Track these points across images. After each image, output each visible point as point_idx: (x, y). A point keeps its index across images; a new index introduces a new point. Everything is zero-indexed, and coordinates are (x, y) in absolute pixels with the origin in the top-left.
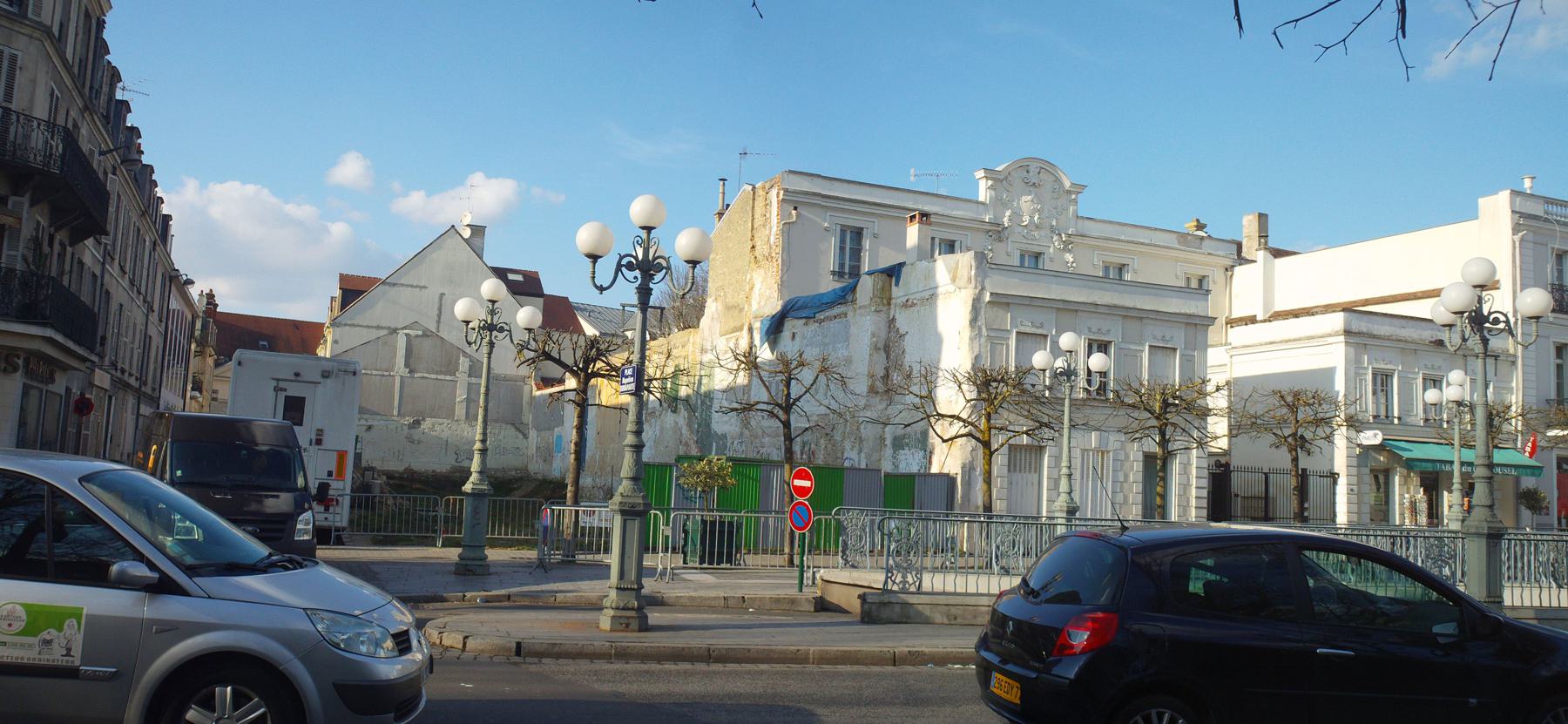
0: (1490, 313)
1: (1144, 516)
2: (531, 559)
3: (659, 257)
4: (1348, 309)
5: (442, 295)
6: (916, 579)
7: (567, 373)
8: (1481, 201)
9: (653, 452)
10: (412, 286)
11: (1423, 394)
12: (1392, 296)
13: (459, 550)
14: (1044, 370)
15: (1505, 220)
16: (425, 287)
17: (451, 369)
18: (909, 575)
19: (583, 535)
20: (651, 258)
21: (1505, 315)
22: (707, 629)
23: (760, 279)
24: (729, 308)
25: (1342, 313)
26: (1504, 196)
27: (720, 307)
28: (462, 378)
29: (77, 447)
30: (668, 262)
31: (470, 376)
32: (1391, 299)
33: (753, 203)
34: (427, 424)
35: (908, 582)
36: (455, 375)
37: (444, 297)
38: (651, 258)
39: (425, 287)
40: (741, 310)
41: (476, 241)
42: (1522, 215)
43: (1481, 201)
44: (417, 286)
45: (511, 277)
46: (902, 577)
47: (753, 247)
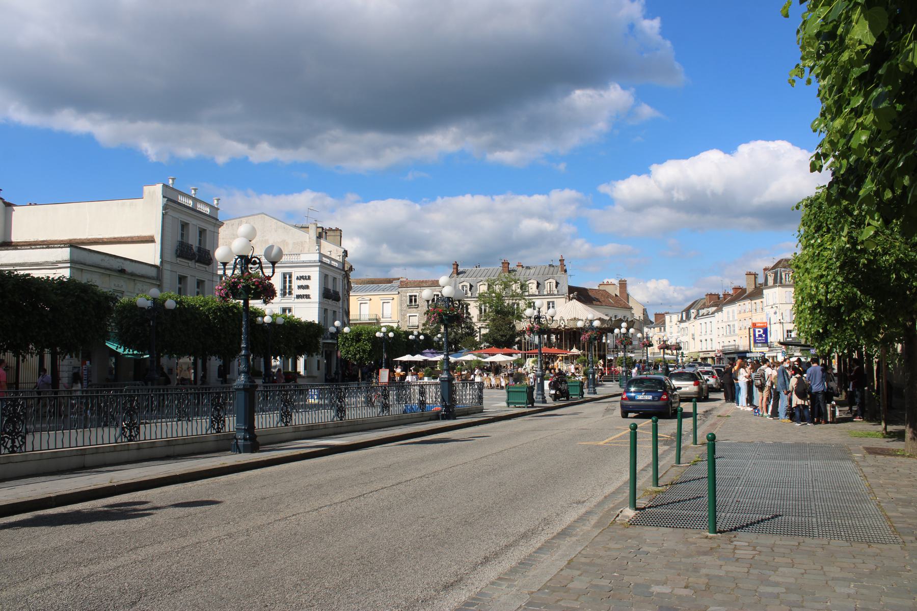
0: (252, 258)
1: (676, 418)
4: (73, 245)
6: (21, 443)
7: (868, 133)
8: (145, 188)
9: (238, 272)
12: (132, 238)
13: (198, 359)
15: (159, 202)
18: (16, 440)
21: (259, 259)
22: (185, 503)
25: (68, 249)
26: (159, 188)
32: (129, 240)
35: (16, 446)
42: (169, 200)
43: (145, 188)
46: (12, 443)
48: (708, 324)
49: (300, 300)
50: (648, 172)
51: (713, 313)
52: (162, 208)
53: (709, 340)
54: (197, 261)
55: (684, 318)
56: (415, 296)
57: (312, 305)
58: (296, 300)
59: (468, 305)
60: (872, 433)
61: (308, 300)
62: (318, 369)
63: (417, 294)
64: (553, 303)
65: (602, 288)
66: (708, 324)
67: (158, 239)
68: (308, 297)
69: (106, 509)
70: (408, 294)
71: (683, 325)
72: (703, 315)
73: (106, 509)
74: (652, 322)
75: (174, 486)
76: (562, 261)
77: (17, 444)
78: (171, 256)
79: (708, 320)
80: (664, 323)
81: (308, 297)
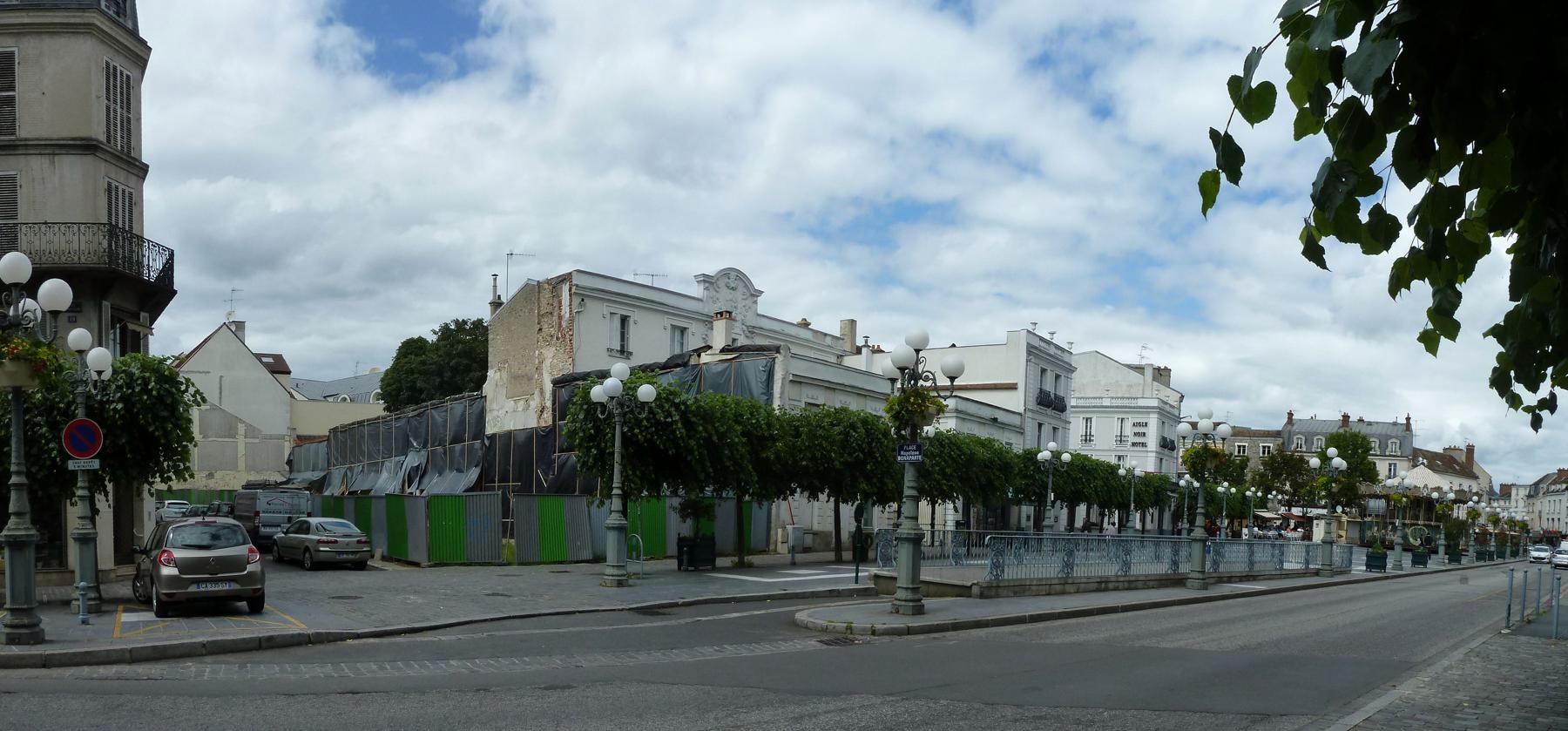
2: (1353, 538)
3: (27, 311)
5: (221, 377)
10: (200, 372)
11: (1188, 422)
14: (1184, 438)
16: (208, 372)
17: (232, 434)
19: (942, 544)
20: (20, 313)
23: (551, 355)
24: (515, 378)
27: (505, 375)
28: (241, 441)
29: (253, 498)
30: (933, 375)
31: (245, 437)
33: (539, 295)
34: (218, 475)
36: (235, 437)
37: (223, 379)
38: (20, 313)
39: (208, 372)
40: (530, 379)
41: (239, 334)
44: (203, 372)
45: (265, 360)
47: (540, 329)
48: (1557, 502)
49: (1135, 448)
50: (175, 292)
51: (1563, 491)
52: (1489, 374)
53: (1556, 520)
54: (1053, 409)
55: (1532, 493)
56: (1244, 446)
57: (1150, 454)
58: (1132, 449)
59: (1375, 464)
60: (50, 695)
61: (1144, 449)
62: (1152, 522)
63: (1247, 444)
64: (1395, 464)
65: (1448, 453)
66: (1557, 502)
67: (1021, 387)
68: (1144, 445)
69: (1433, 651)
70: (1236, 444)
71: (1531, 501)
72: (1552, 492)
73: (1433, 651)
74: (325, 477)
75: (978, 630)
76: (1408, 419)
77: (999, 572)
78: (1032, 405)
79: (1557, 498)
80: (1510, 496)
81: (1144, 445)
